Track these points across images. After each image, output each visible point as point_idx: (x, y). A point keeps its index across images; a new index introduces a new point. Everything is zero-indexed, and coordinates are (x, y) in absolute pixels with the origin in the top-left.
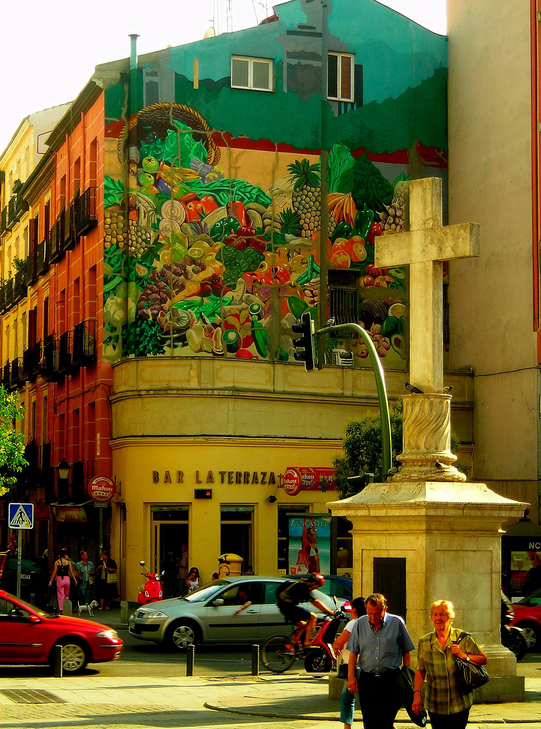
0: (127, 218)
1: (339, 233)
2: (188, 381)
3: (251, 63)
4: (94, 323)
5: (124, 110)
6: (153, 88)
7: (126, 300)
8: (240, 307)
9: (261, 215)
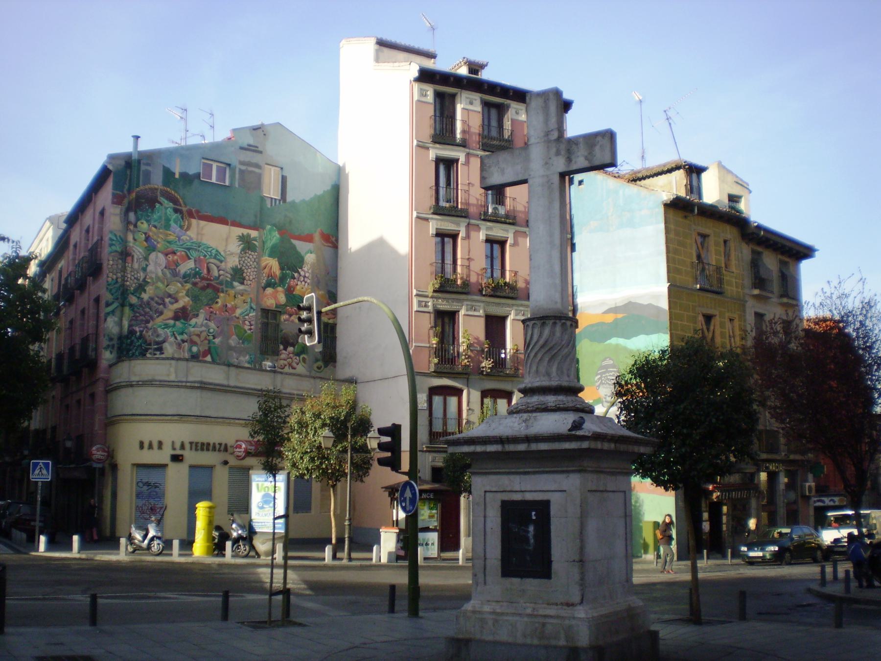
0: (124, 261)
1: (269, 285)
2: (168, 375)
3: (215, 166)
4: (97, 335)
5: (126, 187)
6: (148, 174)
7: (121, 320)
8: (201, 329)
9: (218, 267)
